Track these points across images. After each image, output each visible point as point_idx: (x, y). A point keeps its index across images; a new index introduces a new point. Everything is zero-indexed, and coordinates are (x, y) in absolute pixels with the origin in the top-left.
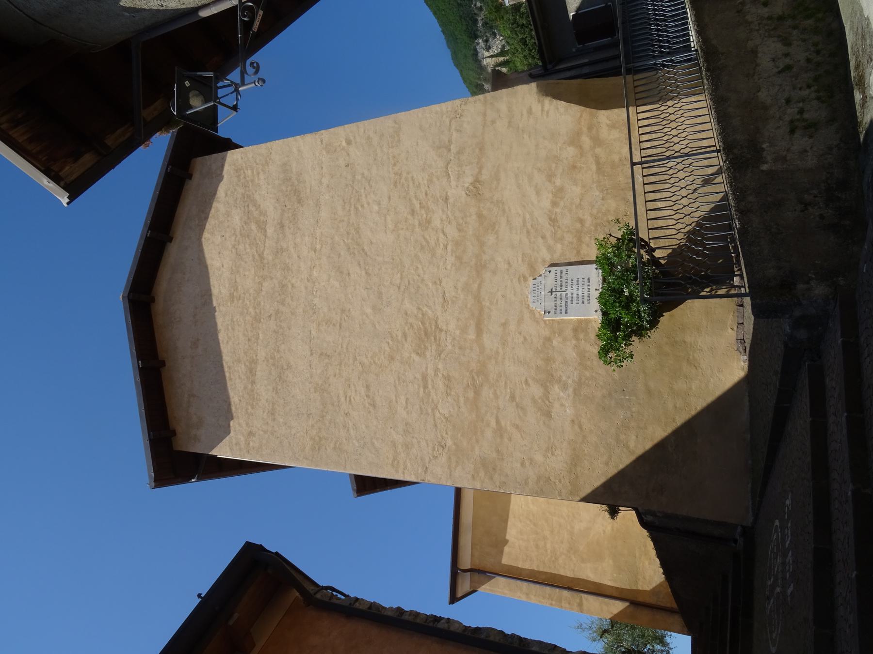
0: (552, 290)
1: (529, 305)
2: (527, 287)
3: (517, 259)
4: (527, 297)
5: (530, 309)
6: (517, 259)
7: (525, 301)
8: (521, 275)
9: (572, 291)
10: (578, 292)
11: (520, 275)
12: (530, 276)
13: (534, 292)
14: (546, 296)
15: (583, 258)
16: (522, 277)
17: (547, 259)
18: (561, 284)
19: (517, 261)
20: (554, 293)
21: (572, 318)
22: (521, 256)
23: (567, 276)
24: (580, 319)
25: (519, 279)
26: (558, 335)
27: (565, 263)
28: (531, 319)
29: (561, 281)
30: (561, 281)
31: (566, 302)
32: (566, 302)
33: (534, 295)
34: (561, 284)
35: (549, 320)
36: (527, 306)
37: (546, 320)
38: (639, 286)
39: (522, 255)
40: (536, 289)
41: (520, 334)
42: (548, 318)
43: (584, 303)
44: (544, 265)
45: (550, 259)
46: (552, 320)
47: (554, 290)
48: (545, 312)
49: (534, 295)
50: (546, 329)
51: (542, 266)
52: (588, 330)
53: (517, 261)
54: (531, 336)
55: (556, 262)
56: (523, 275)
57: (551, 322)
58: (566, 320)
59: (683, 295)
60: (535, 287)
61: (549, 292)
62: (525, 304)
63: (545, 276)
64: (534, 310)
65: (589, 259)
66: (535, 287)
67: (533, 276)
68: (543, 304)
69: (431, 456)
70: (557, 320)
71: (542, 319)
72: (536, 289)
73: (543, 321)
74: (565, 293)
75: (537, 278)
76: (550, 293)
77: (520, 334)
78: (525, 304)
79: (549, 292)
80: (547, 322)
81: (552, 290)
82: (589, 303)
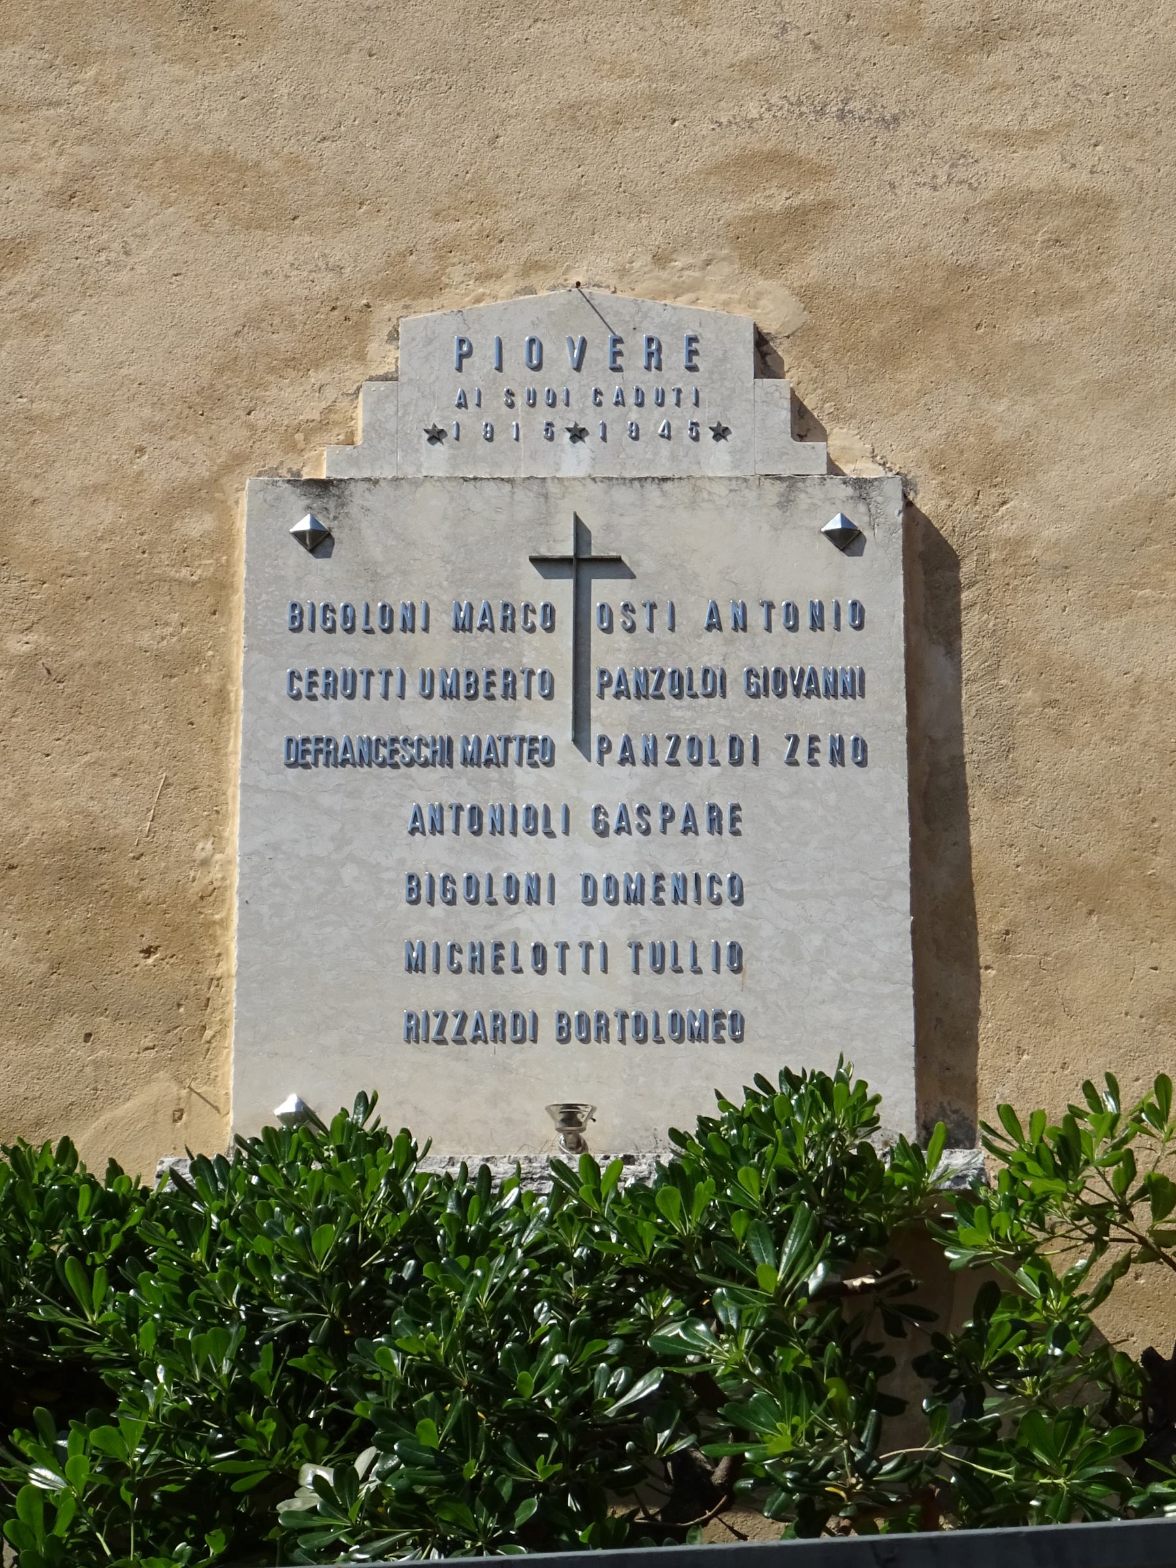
0: (613, 565)
1: (433, 287)
2: (660, 259)
3: (1039, 136)
4: (531, 267)
5: (387, 309)
6: (1039, 136)
7: (492, 237)
8: (828, 190)
9: (583, 820)
10: (570, 889)
11: (818, 172)
12: (808, 297)
13: (599, 353)
14: (526, 503)
15: (1005, 948)
16: (807, 196)
17: (1020, 503)
18: (680, 685)
19: (1005, 138)
20: (561, 590)
21: (234, 829)
22: (1078, 180)
23: (775, 751)
24: (211, 929)
25: (778, 160)
26: (28, 662)
27: (956, 731)
28: (253, 322)
29: (716, 684)
30: (716, 684)
31: (444, 752)
32: (444, 752)
33: (559, 357)
34: (680, 685)
35: (222, 542)
36: (423, 265)
37: (225, 513)
38: (1085, 176)
39: (1081, 199)
40: (635, 373)
41: (67, 198)
42: (242, 525)
43: (415, 966)
44: (939, 466)
45: (1017, 545)
46: (221, 586)
47: (603, 590)
48: (323, 486)
49: (559, 357)
50: (106, 513)
51: (930, 438)
52: (70, 1025)
53: (1005, 138)
54: (33, 322)
55: (971, 621)
56: (826, 207)
57: (204, 569)
58: (217, 749)
59: (793, 680)
60: (654, 353)
61: (581, 532)
62: (445, 250)
63: (793, 481)
64: (361, 356)
65: (986, 1027)
66: (654, 353)
67: (796, 335)
68: (435, 461)
69: (167, 1295)
70: (220, 642)
71: (238, 460)
72: (635, 373)
73: (214, 482)
74: (563, 736)
75: (778, 390)
76: (567, 549)
77: (67, 198)
78: (445, 250)
79: (581, 532)
80: (198, 525)
81: (613, 565)
82: (415, 1031)
